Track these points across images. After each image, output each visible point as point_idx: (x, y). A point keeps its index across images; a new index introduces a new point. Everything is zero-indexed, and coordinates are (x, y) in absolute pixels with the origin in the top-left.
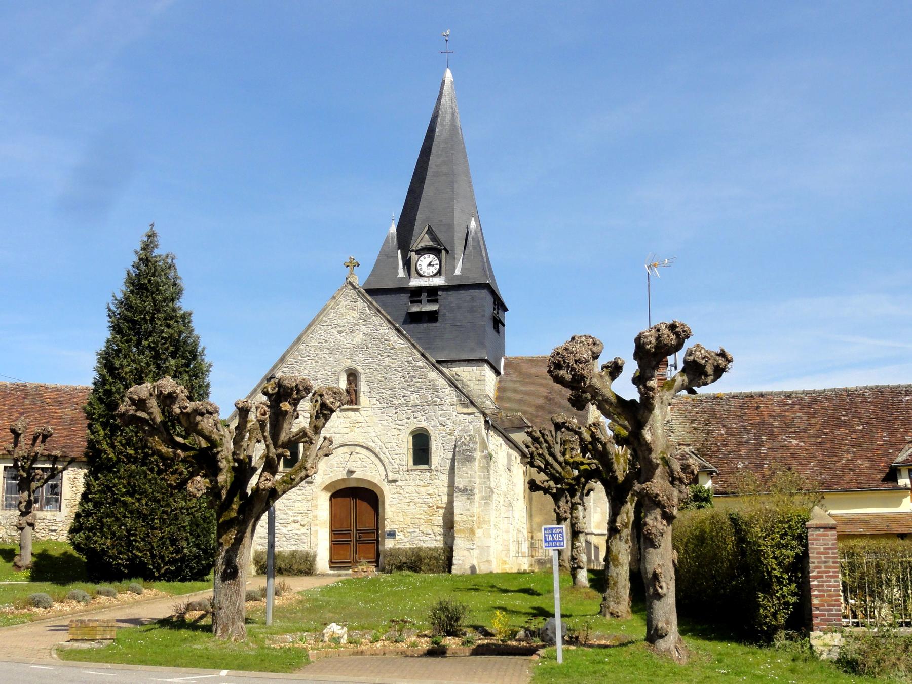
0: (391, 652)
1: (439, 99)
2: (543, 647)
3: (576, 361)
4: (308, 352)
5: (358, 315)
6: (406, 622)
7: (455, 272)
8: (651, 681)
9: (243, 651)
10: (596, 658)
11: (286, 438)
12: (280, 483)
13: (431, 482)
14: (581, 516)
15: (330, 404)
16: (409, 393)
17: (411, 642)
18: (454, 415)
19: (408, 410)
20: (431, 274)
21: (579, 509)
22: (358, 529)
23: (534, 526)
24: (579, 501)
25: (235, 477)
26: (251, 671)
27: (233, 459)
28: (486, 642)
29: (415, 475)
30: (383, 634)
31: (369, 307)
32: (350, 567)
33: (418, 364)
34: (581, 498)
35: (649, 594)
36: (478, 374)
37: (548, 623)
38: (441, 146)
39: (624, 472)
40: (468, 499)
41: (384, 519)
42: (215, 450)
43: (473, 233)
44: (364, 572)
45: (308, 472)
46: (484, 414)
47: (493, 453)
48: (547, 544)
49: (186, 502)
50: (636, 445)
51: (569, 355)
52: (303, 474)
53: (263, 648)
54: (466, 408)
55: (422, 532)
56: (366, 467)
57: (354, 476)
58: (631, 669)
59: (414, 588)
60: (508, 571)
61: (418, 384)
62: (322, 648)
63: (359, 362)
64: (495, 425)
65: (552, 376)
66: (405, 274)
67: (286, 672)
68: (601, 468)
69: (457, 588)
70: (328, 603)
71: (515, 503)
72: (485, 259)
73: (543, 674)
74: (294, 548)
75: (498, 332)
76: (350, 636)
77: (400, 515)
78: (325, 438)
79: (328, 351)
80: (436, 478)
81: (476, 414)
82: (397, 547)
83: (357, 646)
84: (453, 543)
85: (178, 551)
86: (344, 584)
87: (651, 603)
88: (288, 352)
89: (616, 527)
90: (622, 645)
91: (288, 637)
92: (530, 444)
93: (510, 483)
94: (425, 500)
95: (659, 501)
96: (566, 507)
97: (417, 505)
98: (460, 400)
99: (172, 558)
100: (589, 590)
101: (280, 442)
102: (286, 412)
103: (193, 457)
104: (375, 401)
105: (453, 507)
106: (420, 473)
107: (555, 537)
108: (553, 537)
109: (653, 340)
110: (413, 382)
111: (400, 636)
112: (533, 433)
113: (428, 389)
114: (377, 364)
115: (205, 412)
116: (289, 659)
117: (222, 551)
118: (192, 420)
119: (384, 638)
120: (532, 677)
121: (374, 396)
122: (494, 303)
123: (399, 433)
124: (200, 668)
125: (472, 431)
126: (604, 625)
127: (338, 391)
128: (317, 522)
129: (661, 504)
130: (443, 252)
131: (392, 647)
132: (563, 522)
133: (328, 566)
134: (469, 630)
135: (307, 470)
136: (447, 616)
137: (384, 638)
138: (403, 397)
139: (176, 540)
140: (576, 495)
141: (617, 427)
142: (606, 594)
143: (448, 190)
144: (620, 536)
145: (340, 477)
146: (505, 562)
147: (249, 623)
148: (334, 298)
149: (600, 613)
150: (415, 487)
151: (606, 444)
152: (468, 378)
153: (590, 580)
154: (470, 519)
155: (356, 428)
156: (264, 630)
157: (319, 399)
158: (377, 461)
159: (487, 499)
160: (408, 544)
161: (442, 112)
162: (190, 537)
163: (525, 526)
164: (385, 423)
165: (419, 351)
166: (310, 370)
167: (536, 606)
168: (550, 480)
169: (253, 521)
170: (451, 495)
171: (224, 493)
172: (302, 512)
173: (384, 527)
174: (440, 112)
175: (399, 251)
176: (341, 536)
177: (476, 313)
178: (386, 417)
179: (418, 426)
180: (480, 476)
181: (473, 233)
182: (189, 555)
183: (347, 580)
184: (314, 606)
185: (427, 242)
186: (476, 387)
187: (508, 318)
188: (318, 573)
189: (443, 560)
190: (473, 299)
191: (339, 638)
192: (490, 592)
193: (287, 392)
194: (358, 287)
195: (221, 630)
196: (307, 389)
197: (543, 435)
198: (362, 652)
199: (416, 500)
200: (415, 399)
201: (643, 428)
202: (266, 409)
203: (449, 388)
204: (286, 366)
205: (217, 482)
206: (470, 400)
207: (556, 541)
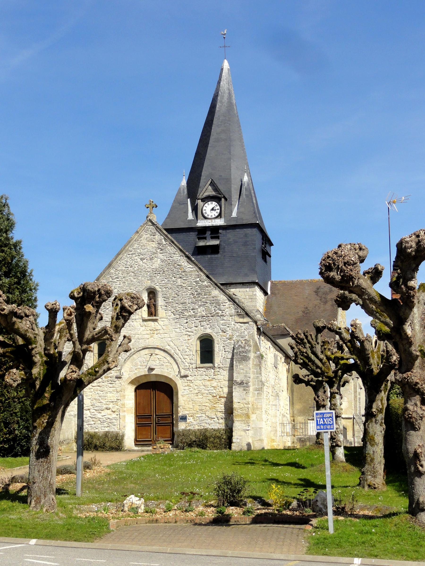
0: (182, 520)
1: (219, 83)
2: (315, 516)
3: (345, 264)
4: (117, 275)
5: (156, 246)
6: (194, 494)
7: (232, 215)
8: (416, 551)
9: (52, 521)
10: (363, 528)
11: (90, 336)
12: (85, 375)
13: (215, 377)
14: (338, 404)
15: (128, 307)
16: (197, 307)
17: (199, 512)
19: (196, 320)
20: (214, 216)
21: (337, 397)
22: (157, 414)
23: (295, 412)
24: (337, 391)
25: (47, 369)
26: (57, 540)
27: (45, 354)
28: (263, 511)
29: (202, 372)
30: (176, 504)
31: (165, 239)
32: (151, 444)
33: (203, 284)
34: (338, 389)
35: (410, 472)
36: (251, 293)
37: (318, 495)
38: (221, 119)
39: (378, 365)
40: (244, 390)
41: (177, 407)
42: (30, 347)
43: (246, 185)
44: (162, 448)
45: (110, 365)
46: (256, 322)
47: (264, 354)
48: (319, 427)
49: (17, 393)
50: (398, 339)
51: (339, 258)
52: (105, 367)
53: (70, 517)
54: (242, 318)
55: (208, 417)
56: (163, 365)
57: (154, 372)
58: (397, 539)
59: (202, 462)
60: (276, 447)
61: (204, 300)
62: (122, 517)
63: (158, 282)
64: (265, 332)
65: (323, 277)
67: (88, 541)
68: (359, 362)
69: (237, 462)
70: (131, 475)
71: (280, 393)
73: (318, 543)
74: (107, 429)
75: (265, 261)
76: (146, 505)
77: (191, 403)
78: (125, 337)
79: (133, 274)
80: (219, 373)
81: (250, 323)
82: (188, 428)
83: (152, 515)
84: (232, 425)
85: (10, 432)
86: (145, 458)
87: (412, 480)
88: (101, 275)
89: (372, 412)
90: (386, 516)
91: (94, 507)
92: (294, 346)
93: (276, 378)
94: (210, 391)
95: (419, 389)
96: (324, 397)
97: (204, 395)
98: (238, 312)
99: (6, 438)
100: (346, 464)
101: (85, 339)
102: (90, 313)
103: (11, 352)
104: (170, 313)
105: (232, 396)
106: (206, 370)
107: (325, 421)
108: (324, 421)
109: (414, 245)
110: (200, 298)
111: (189, 506)
112: (299, 335)
114: (171, 284)
115: (24, 315)
116: (93, 528)
117: (36, 433)
118: (9, 321)
119: (176, 508)
120: (307, 547)
121: (169, 309)
122: (263, 239)
123: (190, 338)
124: (13, 537)
126: (364, 495)
127: (135, 296)
128: (125, 409)
129: (420, 392)
130: (223, 199)
131: (183, 516)
132: (321, 408)
133: (134, 444)
134: (248, 500)
135: (109, 364)
136: (230, 489)
137: (176, 508)
138: (192, 309)
139: (9, 423)
140: (334, 386)
141: (379, 325)
142: (364, 469)
144: (376, 420)
145: (143, 374)
146: (273, 440)
147: (62, 493)
148: (137, 232)
149: (359, 485)
150: (202, 381)
151: (363, 342)
152: (243, 297)
153: (346, 455)
154: (246, 406)
156: (72, 501)
157: (119, 303)
158: (172, 361)
159: (260, 390)
160: (196, 426)
161: (221, 93)
162: (20, 421)
163: (288, 412)
164: (178, 330)
165: (205, 274)
166: (119, 289)
167: (303, 478)
168: (311, 375)
169: (63, 406)
171: (38, 384)
172: (113, 401)
173: (177, 412)
174: (220, 93)
175: (189, 200)
176: (144, 420)
177: (249, 247)
178: (179, 326)
179: (204, 333)
180: (253, 372)
181: (246, 185)
182: (20, 436)
183: (147, 455)
184: (119, 478)
185: (210, 192)
186: (249, 304)
187: (273, 251)
188: (126, 449)
189: (224, 439)
191: (137, 508)
192: (263, 465)
193: (91, 296)
194: (156, 223)
195: (35, 501)
196: (109, 294)
197: (307, 337)
198: (157, 520)
199: (203, 391)
200: (201, 311)
201: (404, 324)
202: (72, 310)
203: (229, 303)
205: (31, 374)
207: (327, 425)
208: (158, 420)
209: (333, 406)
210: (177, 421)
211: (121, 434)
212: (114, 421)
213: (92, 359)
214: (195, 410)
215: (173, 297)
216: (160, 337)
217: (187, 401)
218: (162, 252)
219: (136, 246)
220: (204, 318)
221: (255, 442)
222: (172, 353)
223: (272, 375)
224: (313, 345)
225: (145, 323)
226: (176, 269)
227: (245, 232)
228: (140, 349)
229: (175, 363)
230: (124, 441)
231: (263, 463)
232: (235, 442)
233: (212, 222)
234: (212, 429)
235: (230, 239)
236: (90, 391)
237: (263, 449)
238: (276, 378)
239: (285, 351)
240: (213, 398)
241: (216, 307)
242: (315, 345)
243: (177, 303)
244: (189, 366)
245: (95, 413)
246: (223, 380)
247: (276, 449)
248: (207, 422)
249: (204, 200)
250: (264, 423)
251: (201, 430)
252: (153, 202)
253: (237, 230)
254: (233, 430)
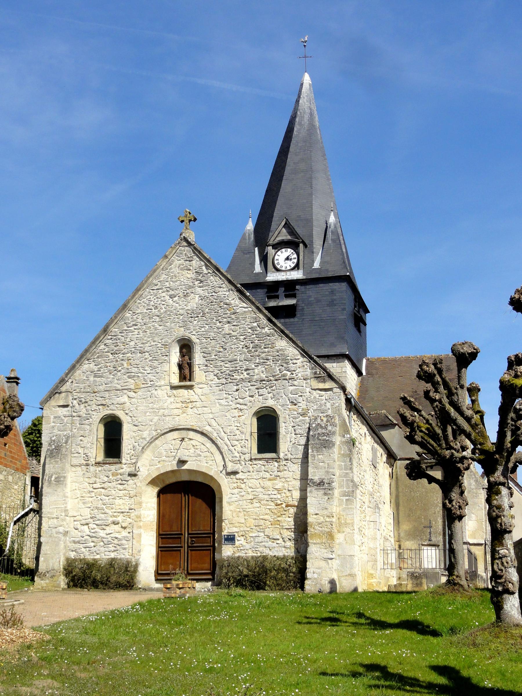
1: (298, 101)
5: (193, 276)
13: (279, 474)
14: (506, 506)
16: (253, 366)
18: (307, 392)
19: (252, 385)
20: (289, 268)
22: (190, 532)
23: (402, 535)
24: (502, 479)
29: (259, 466)
31: (206, 266)
33: (263, 331)
38: (300, 145)
40: (325, 494)
41: (221, 521)
44: (180, 588)
54: (322, 382)
55: (268, 537)
57: (186, 467)
61: (263, 355)
63: (194, 330)
66: (261, 270)
72: (345, 255)
74: (112, 555)
75: (359, 331)
77: (241, 514)
79: (158, 319)
80: (286, 468)
81: (335, 390)
82: (237, 555)
84: (306, 551)
88: (112, 321)
93: (375, 482)
94: (272, 496)
96: (460, 501)
97: (262, 502)
104: (212, 376)
105: (306, 504)
106: (265, 463)
110: (257, 353)
112: (425, 367)
113: (275, 361)
114: (215, 332)
121: (211, 370)
123: (241, 414)
125: (330, 411)
128: (141, 524)
130: (301, 245)
133: (153, 578)
138: (246, 370)
140: (496, 469)
143: (307, 186)
145: (169, 469)
146: (371, 576)
148: (166, 257)
150: (260, 481)
154: (328, 519)
155: (189, 409)
158: (214, 449)
160: (250, 551)
161: (300, 113)
163: (392, 534)
164: (223, 402)
165: (266, 316)
166: (137, 342)
170: (303, 490)
173: (221, 530)
175: (256, 249)
176: (170, 541)
178: (225, 395)
179: (264, 405)
180: (340, 466)
185: (284, 236)
187: (369, 318)
188: (140, 586)
189: (294, 573)
190: (332, 292)
194: (193, 243)
197: (440, 371)
199: (261, 496)
200: (259, 372)
203: (302, 359)
204: (109, 337)
206: (327, 372)
208: (192, 541)
209: (497, 511)
210: (220, 544)
211: (134, 563)
212: (124, 542)
213: (95, 446)
214: (248, 525)
215: (216, 351)
216: (197, 412)
217: (235, 511)
218: (201, 284)
219: (163, 277)
220: (264, 382)
221: (343, 578)
222: (214, 438)
223: (369, 476)
224: (453, 389)
225: (175, 392)
226: (222, 310)
227: (331, 288)
228: (166, 431)
229: (218, 452)
230: (138, 574)
231: (355, 620)
232: (310, 579)
233: (286, 275)
234: (275, 556)
235: (310, 297)
236: (89, 495)
237: (356, 590)
238: (375, 482)
239: (386, 445)
240: (276, 507)
241: (282, 366)
242: (456, 389)
243: (223, 361)
244: (240, 457)
245: (97, 530)
246: (292, 479)
247: (378, 592)
248: (267, 544)
249: (276, 246)
250: (356, 547)
251: (257, 557)
252: (190, 213)
253: (321, 285)
254: (308, 559)
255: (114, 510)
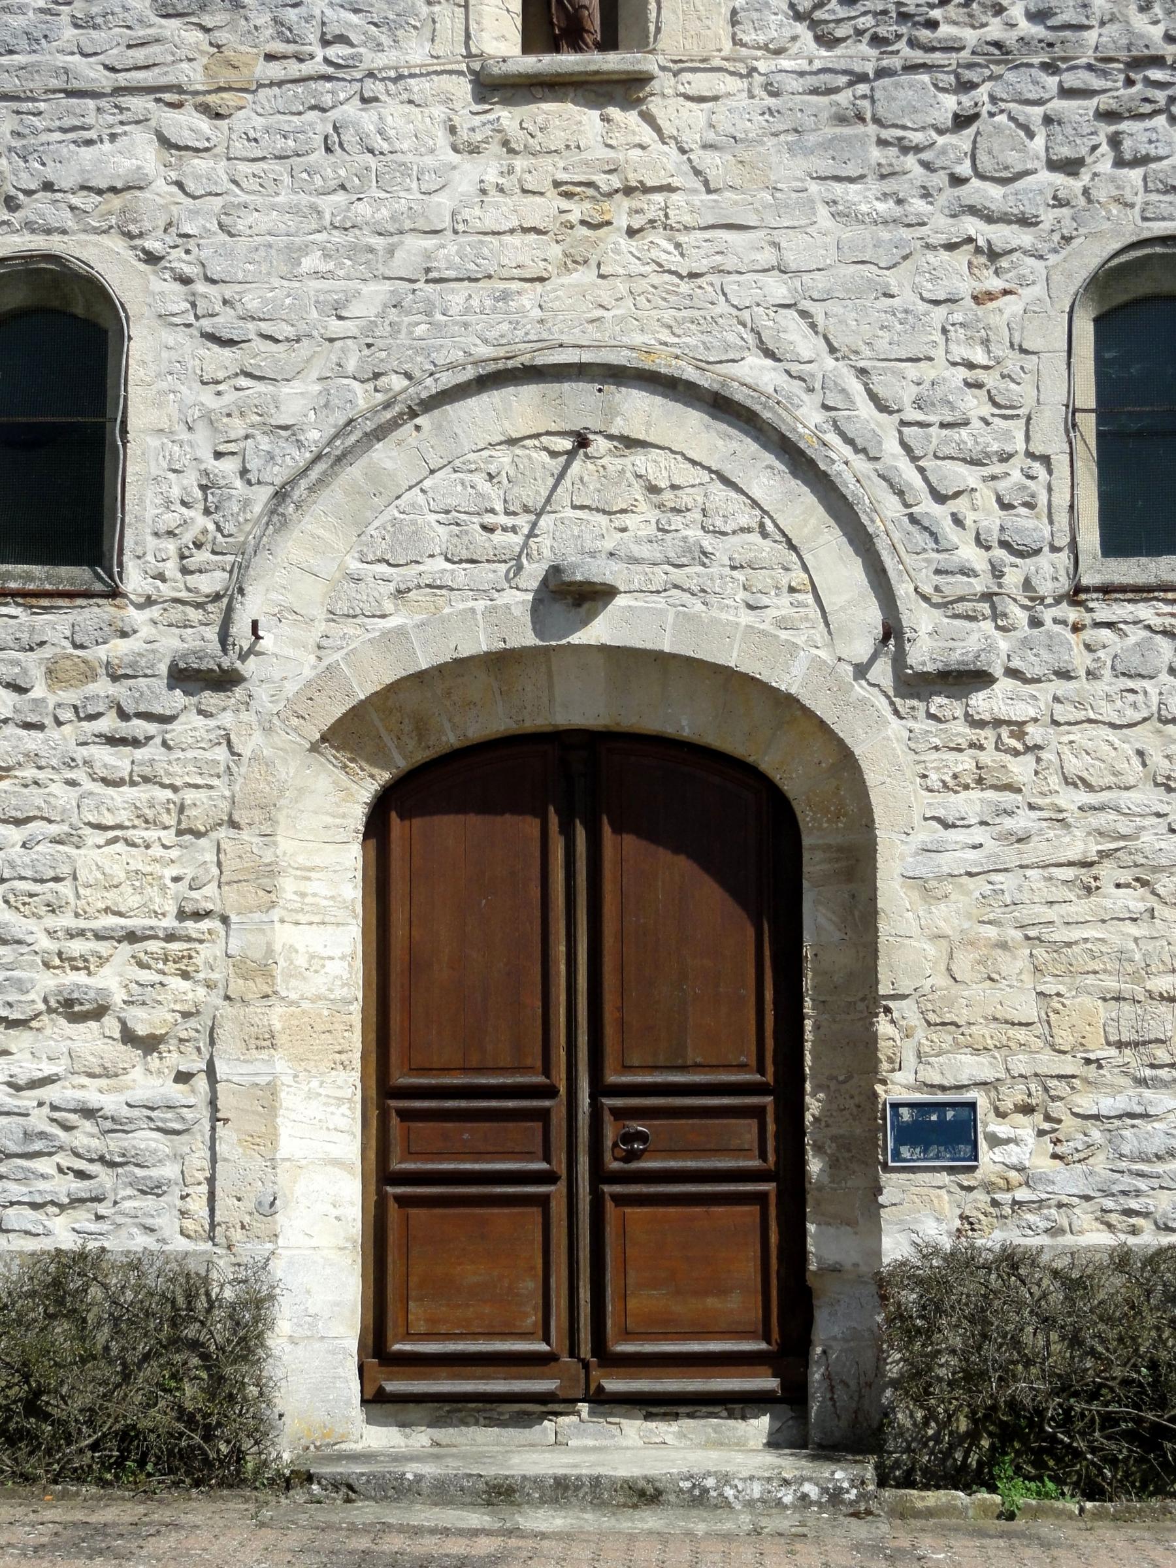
19: (1067, 93)
29: (1136, 635)
128: (276, 1017)
145: (480, 642)
150: (1144, 737)
155: (615, 238)
160: (1083, 1216)
172: (135, 923)
176: (467, 1132)
178: (876, 154)
255: (66, 921)
